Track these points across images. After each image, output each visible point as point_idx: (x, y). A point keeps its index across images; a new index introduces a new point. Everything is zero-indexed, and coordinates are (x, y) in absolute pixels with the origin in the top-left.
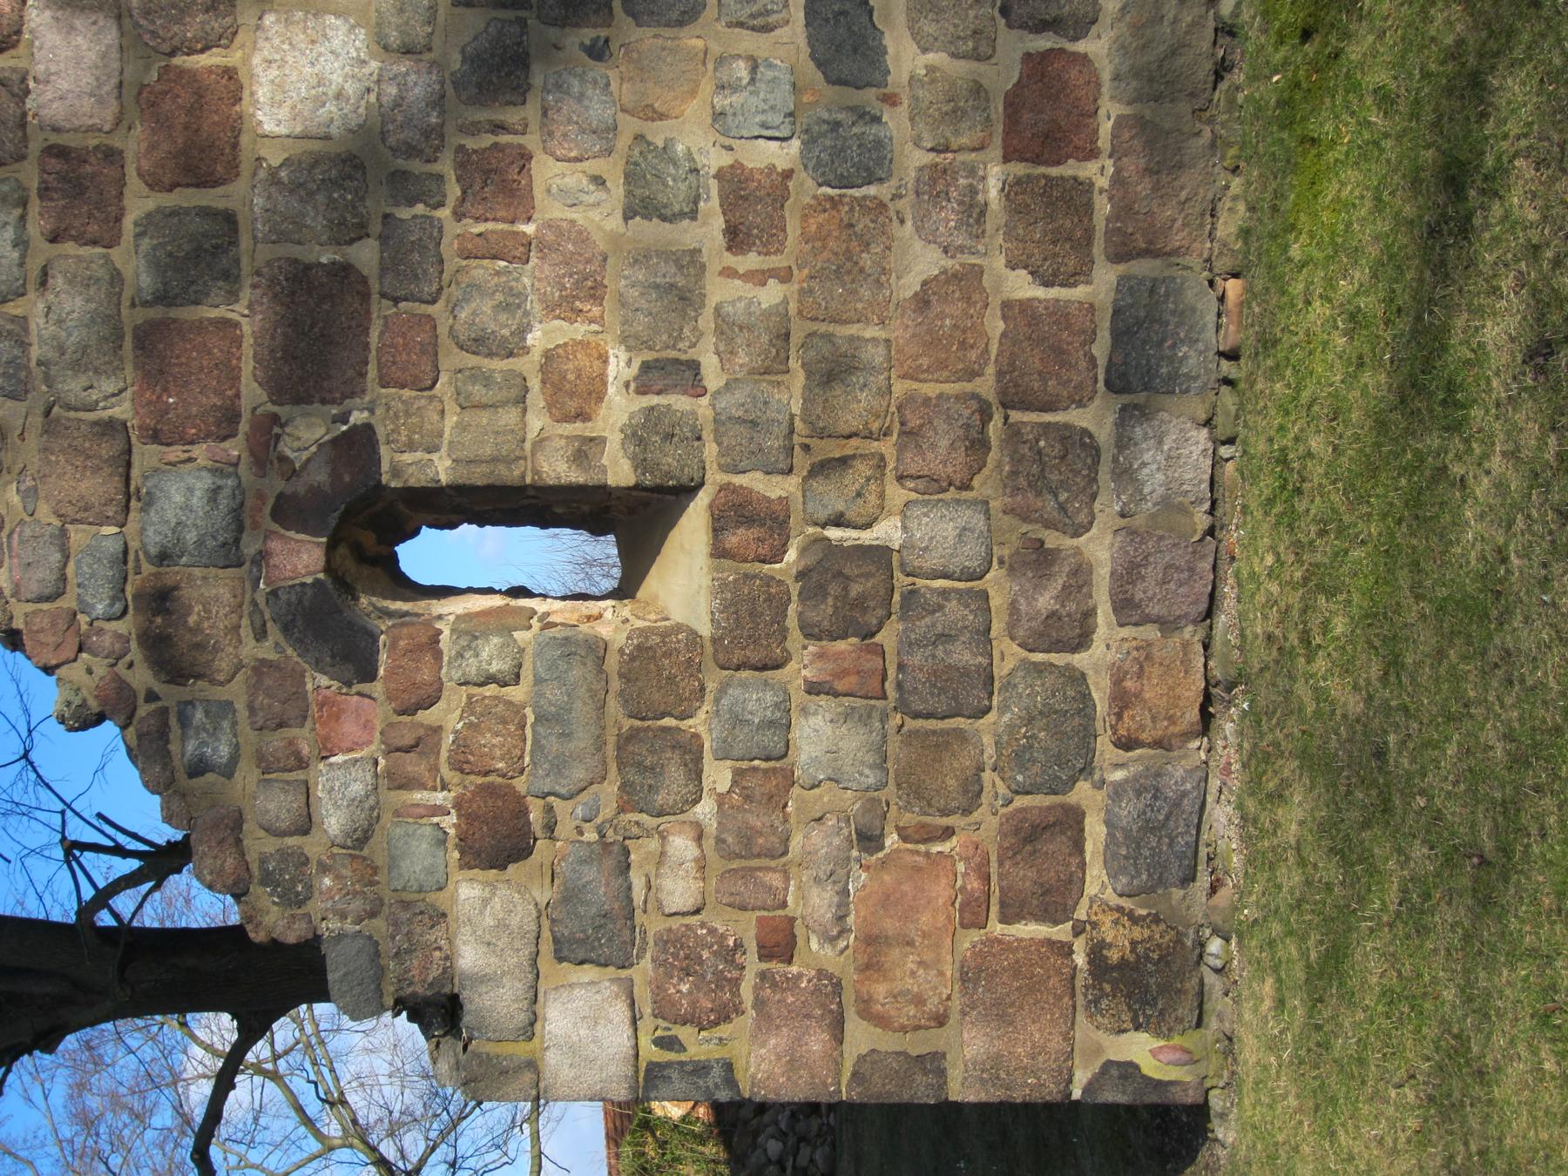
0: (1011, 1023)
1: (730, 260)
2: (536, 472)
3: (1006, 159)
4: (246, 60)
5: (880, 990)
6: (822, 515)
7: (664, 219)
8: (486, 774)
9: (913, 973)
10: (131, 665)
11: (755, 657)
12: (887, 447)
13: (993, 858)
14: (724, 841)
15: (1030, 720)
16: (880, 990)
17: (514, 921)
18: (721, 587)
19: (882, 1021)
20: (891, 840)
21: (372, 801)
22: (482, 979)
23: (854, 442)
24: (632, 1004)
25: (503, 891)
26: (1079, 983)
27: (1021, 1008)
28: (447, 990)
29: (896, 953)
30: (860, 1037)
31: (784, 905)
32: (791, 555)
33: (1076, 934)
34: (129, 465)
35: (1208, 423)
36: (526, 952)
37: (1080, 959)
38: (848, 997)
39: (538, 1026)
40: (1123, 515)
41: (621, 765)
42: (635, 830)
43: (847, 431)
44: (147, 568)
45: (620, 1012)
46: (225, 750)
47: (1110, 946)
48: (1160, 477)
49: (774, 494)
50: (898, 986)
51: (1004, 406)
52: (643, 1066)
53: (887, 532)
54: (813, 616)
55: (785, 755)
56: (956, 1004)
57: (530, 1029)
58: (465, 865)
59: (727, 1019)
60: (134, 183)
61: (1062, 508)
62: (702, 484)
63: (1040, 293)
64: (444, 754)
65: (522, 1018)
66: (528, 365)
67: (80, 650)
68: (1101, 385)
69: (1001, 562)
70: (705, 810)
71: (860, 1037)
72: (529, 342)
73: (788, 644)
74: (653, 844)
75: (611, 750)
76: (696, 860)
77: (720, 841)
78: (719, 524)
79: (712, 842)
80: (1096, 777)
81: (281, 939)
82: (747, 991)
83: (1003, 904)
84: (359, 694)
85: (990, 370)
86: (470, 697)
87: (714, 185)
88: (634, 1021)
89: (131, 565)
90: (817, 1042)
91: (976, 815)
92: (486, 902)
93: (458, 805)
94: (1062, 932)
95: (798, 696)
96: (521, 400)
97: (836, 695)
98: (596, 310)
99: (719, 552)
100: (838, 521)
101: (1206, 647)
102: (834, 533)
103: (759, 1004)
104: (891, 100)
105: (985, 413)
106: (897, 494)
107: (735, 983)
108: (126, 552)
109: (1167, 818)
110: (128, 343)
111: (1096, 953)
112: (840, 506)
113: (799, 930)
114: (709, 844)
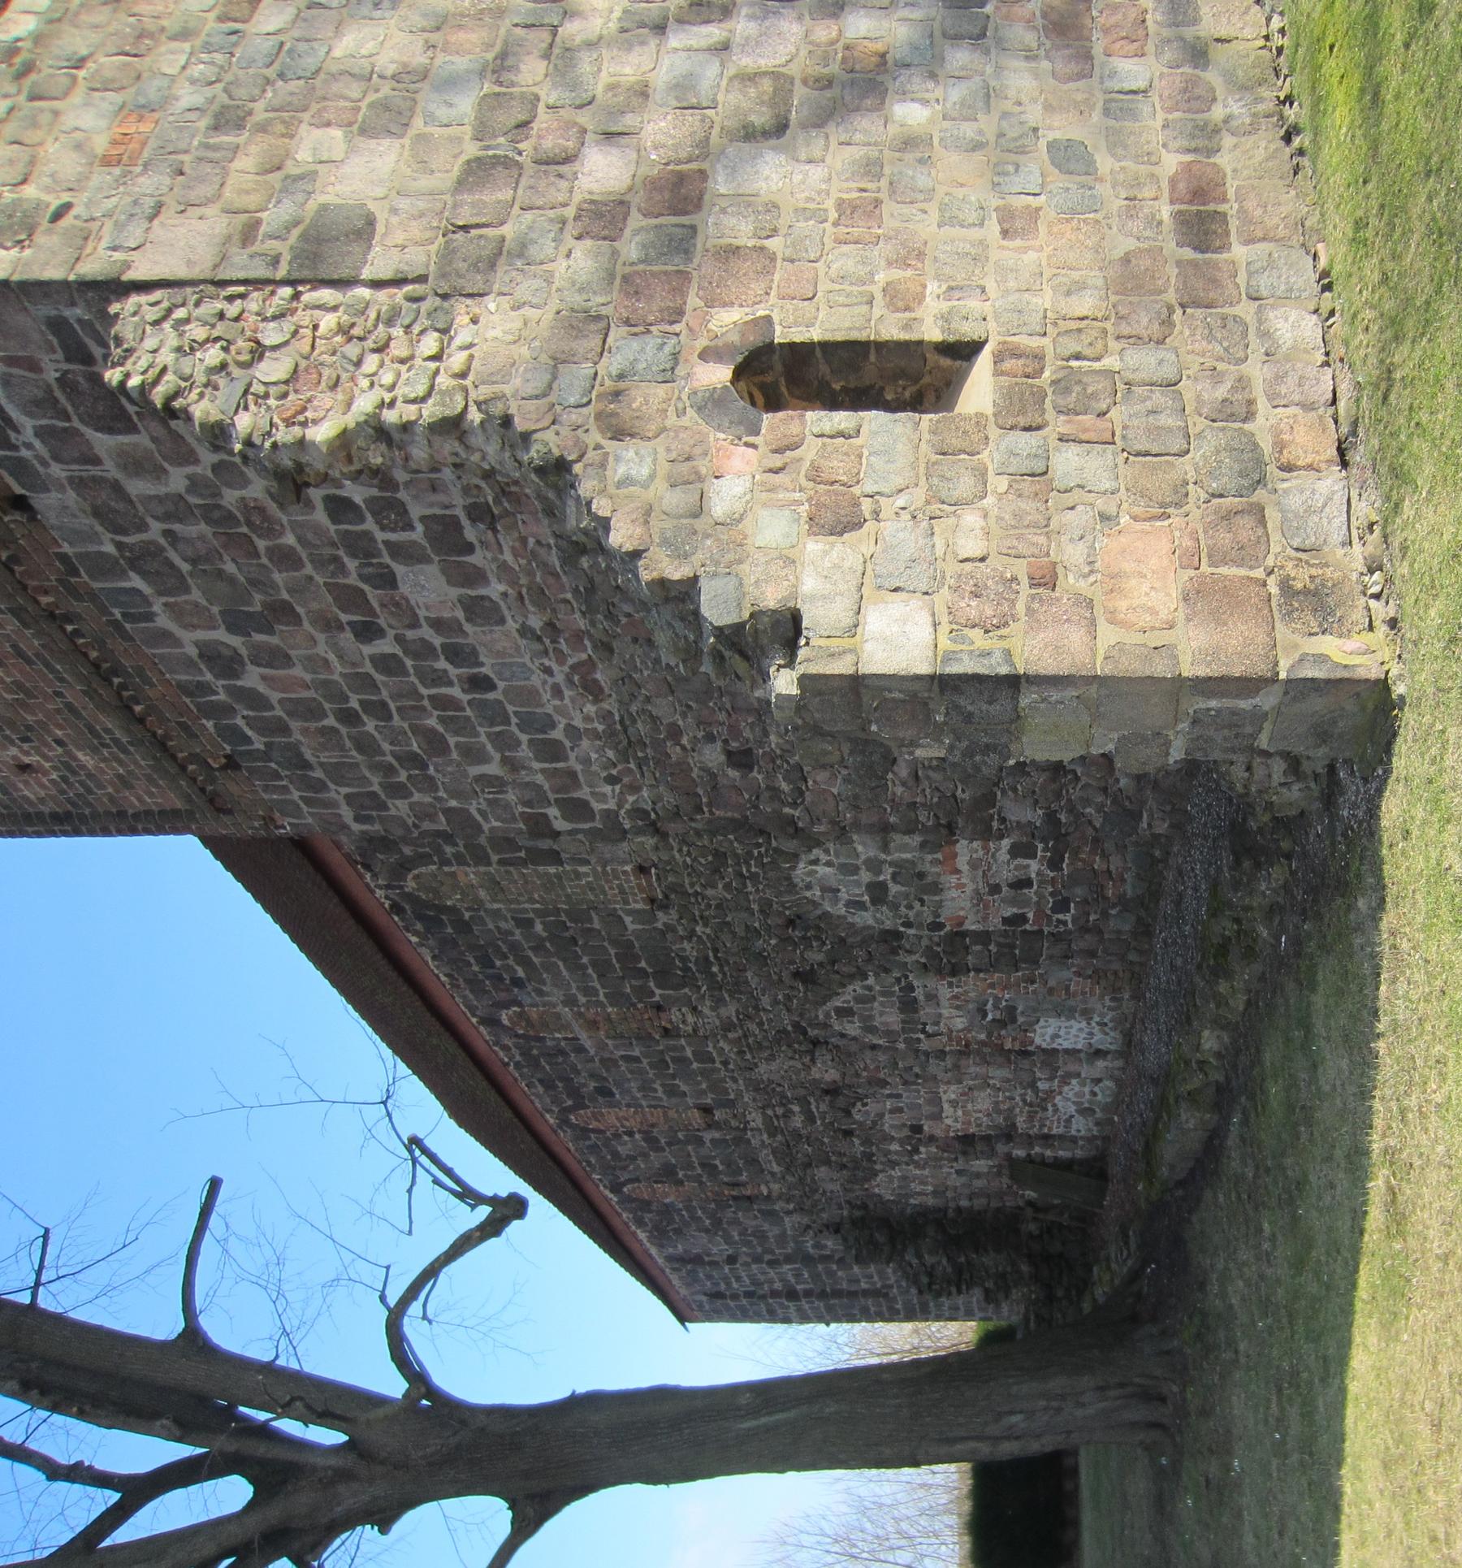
0: (1225, 624)
1: (1005, 243)
2: (877, 333)
3: (1172, 202)
4: (713, 166)
5: (1123, 605)
6: (1067, 353)
7: (963, 226)
8: (832, 483)
9: (1147, 594)
10: (587, 431)
11: (1023, 421)
12: (1108, 325)
13: (1200, 531)
14: (1002, 519)
15: (1218, 452)
16: (1123, 605)
17: (847, 564)
18: (998, 388)
19: (1122, 624)
20: (1125, 519)
21: (748, 497)
22: (813, 598)
23: (1086, 322)
24: (933, 615)
25: (839, 546)
26: (1274, 603)
27: (1231, 614)
28: (791, 604)
29: (1133, 582)
30: (1108, 635)
31: (1048, 554)
32: (1047, 374)
33: (1269, 574)
34: (606, 335)
35: (1316, 311)
36: (855, 583)
37: (1274, 590)
38: (1098, 611)
39: (860, 629)
40: (1267, 355)
41: (928, 477)
42: (939, 513)
43: (1081, 315)
44: (608, 383)
45: (925, 619)
46: (645, 471)
47: (1294, 579)
48: (1289, 335)
49: (1035, 345)
50: (1136, 602)
51: (1183, 306)
52: (940, 653)
53: (1110, 362)
54: (1061, 402)
55: (1046, 473)
56: (1180, 616)
57: (853, 629)
58: (811, 533)
59: (1006, 624)
60: (634, 212)
61: (1226, 349)
62: (986, 341)
63: (1200, 256)
64: (803, 473)
65: (848, 621)
66: (877, 290)
67: (553, 423)
68: (1244, 296)
69: (1189, 377)
70: (989, 501)
71: (1108, 635)
72: (876, 278)
73: (1047, 416)
74: (952, 520)
75: (922, 470)
76: (983, 529)
77: (999, 518)
78: (998, 359)
79: (994, 520)
80: (1270, 486)
81: (670, 577)
82: (1020, 607)
83: (1210, 556)
84: (747, 445)
85: (1172, 290)
86: (824, 444)
87: (994, 215)
88: (935, 625)
89: (598, 382)
90: (1076, 637)
91: (1186, 508)
92: (825, 553)
93: (809, 500)
94: (1259, 573)
95: (1053, 442)
96: (870, 303)
97: (1081, 442)
98: (920, 265)
99: (997, 373)
100: (1078, 357)
101: (1336, 422)
102: (1074, 363)
103: (1030, 611)
104: (1101, 180)
105: (1171, 310)
106: (1113, 345)
107: (1013, 602)
108: (596, 374)
109: (1324, 506)
110: (618, 281)
111: (1285, 585)
112: (1079, 349)
113: (1060, 570)
114: (992, 521)
